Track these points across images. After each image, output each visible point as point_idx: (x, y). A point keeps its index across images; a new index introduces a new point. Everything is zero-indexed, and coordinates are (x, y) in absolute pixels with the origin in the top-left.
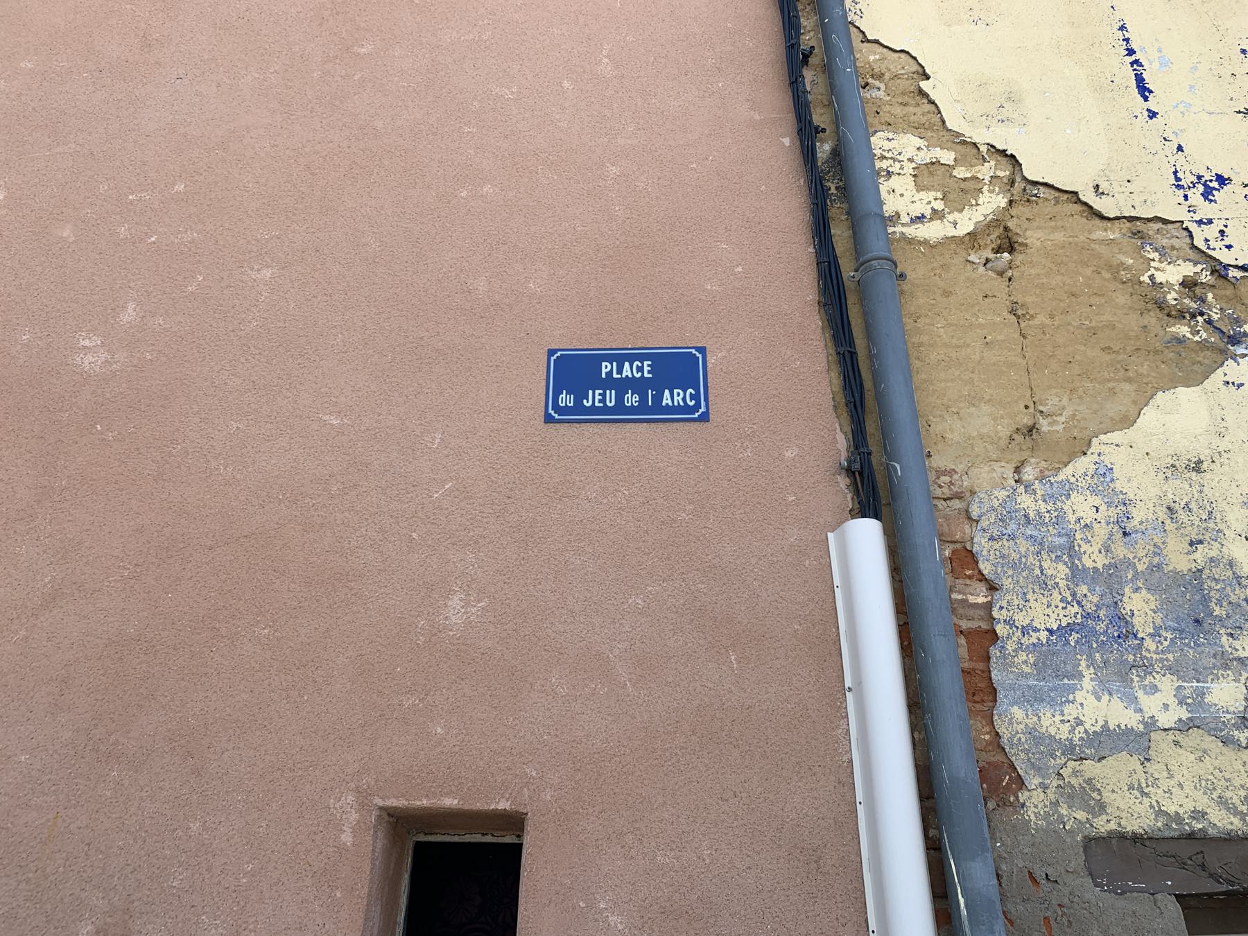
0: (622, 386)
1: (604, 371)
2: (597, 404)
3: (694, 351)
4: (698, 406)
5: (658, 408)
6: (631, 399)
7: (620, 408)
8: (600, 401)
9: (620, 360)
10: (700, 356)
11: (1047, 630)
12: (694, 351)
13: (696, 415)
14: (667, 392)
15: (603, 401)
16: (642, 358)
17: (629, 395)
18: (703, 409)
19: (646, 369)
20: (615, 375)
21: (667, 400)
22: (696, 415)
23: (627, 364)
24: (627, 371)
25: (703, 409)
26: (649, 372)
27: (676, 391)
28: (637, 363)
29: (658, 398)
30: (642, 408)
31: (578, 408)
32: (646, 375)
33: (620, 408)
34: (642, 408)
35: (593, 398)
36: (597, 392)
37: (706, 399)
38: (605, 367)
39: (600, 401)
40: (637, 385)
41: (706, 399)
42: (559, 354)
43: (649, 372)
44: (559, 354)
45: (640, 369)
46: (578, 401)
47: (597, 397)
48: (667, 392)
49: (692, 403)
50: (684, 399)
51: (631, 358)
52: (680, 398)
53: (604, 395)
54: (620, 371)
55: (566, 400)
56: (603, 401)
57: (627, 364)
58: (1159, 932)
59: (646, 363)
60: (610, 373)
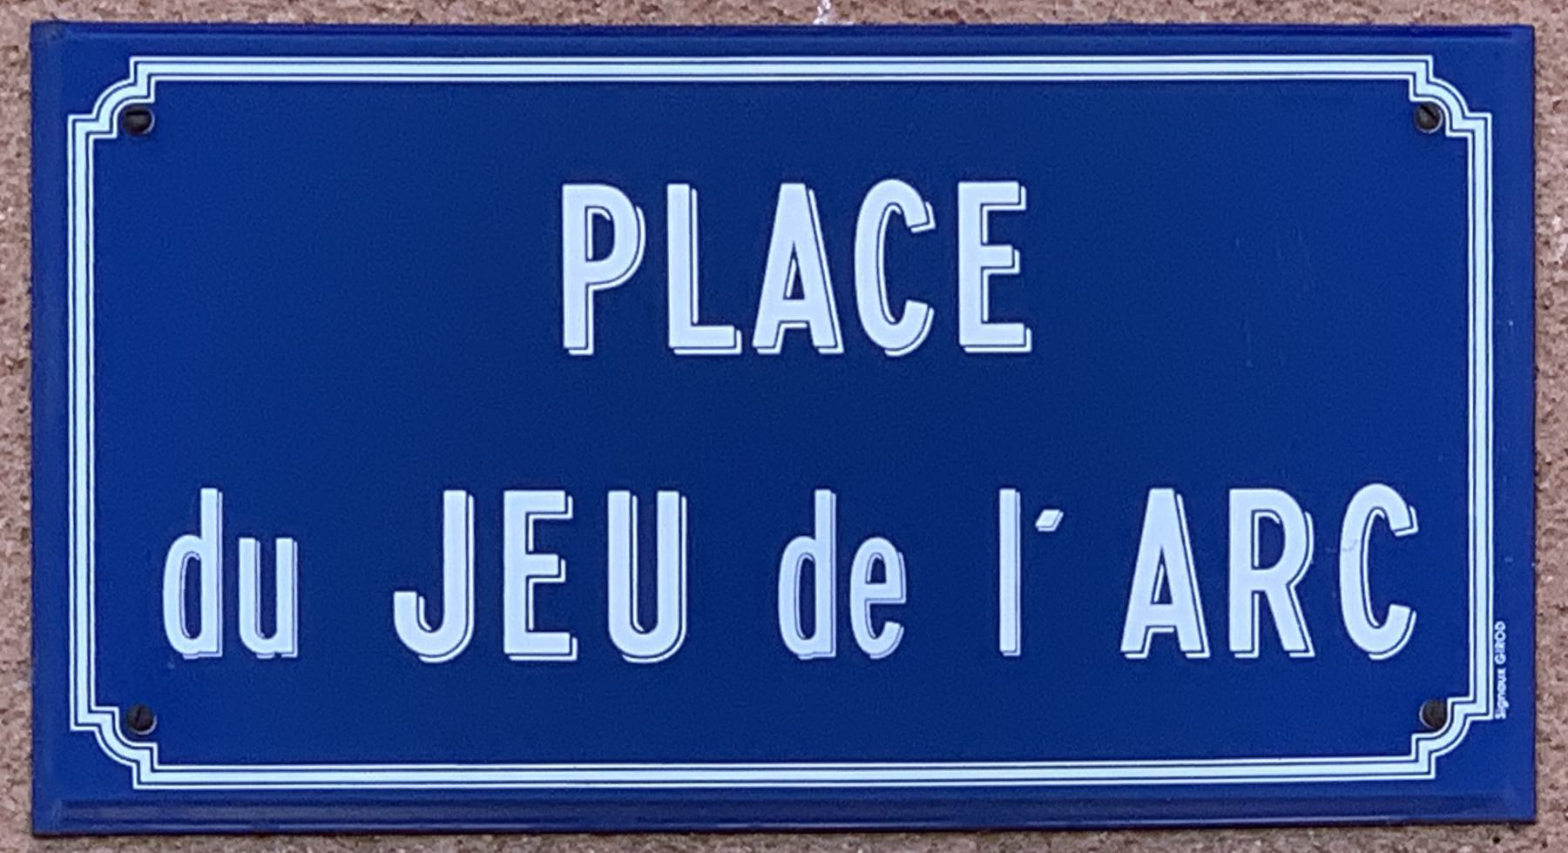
0: (756, 443)
1: (582, 277)
2: (523, 641)
3: (1419, 76)
4: (1435, 665)
5: (1085, 683)
6: (840, 589)
7: (733, 679)
8: (550, 608)
9: (733, 153)
10: (1471, 127)
11: (1557, 607)
12: (1419, 76)
13: (1421, 760)
14: (1164, 512)
15: (572, 605)
16: (938, 138)
17: (819, 546)
18: (1479, 702)
19: (980, 260)
20: (690, 334)
21: (1158, 608)
22: (1421, 760)
23: (795, 206)
24: (794, 302)
25: (1479, 702)
26: (1005, 299)
27: (1246, 504)
28: (892, 197)
29: (1084, 576)
30: (935, 684)
31: (348, 685)
32: (980, 333)
33: (733, 679)
34: (935, 684)
35: (483, 579)
36: (524, 507)
37: (1517, 604)
38: (597, 238)
39: (550, 608)
40: (878, 431)
41: (1517, 604)
42: (144, 78)
43: (1005, 299)
44: (144, 78)
45: (921, 266)
46: (344, 609)
47: (527, 568)
48: (1164, 512)
49: (1382, 636)
50: (1318, 592)
51: (841, 143)
52: (1280, 581)
53: (577, 540)
54: (731, 290)
55: (230, 591)
56: (572, 605)
57: (795, 206)
58: (6, 729)
59: (978, 198)
60: (633, 308)
